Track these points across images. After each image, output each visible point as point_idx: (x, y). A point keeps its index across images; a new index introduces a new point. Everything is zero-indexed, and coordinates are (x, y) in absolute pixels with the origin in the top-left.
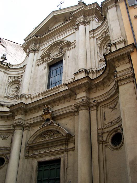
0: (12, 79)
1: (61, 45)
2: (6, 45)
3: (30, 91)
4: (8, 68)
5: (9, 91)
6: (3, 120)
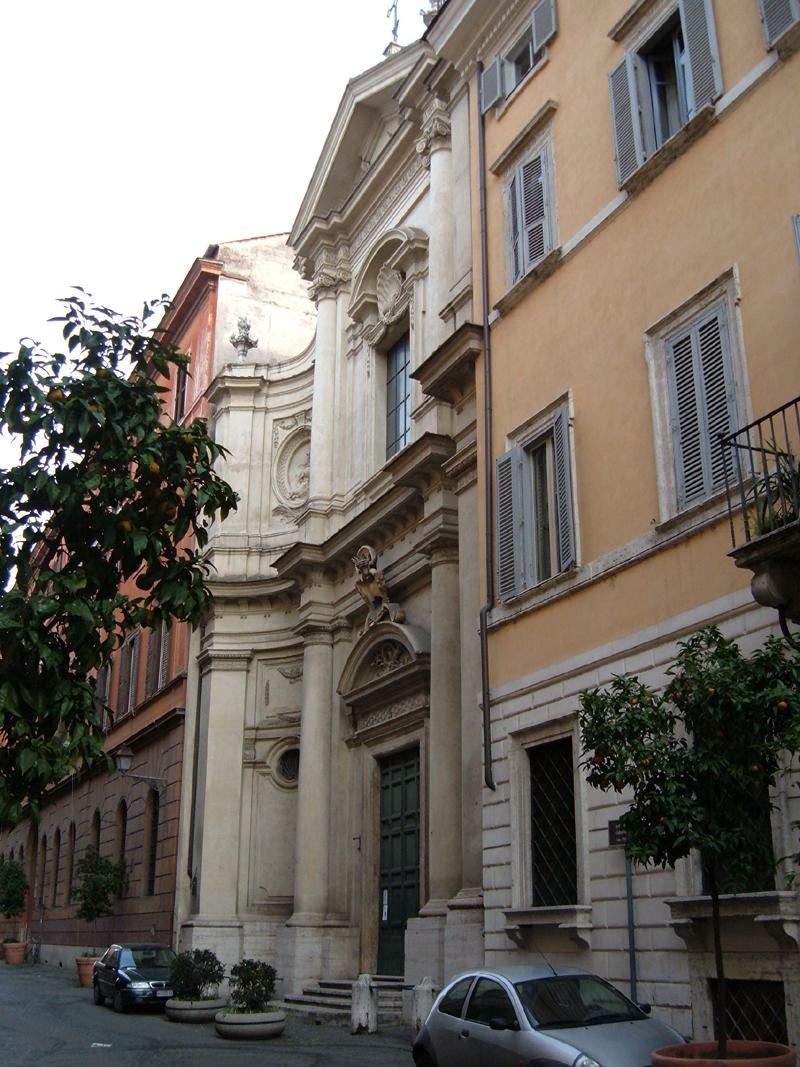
0: (288, 428)
1: (394, 260)
2: (249, 267)
6: (279, 610)
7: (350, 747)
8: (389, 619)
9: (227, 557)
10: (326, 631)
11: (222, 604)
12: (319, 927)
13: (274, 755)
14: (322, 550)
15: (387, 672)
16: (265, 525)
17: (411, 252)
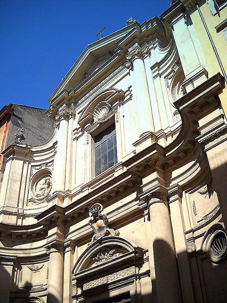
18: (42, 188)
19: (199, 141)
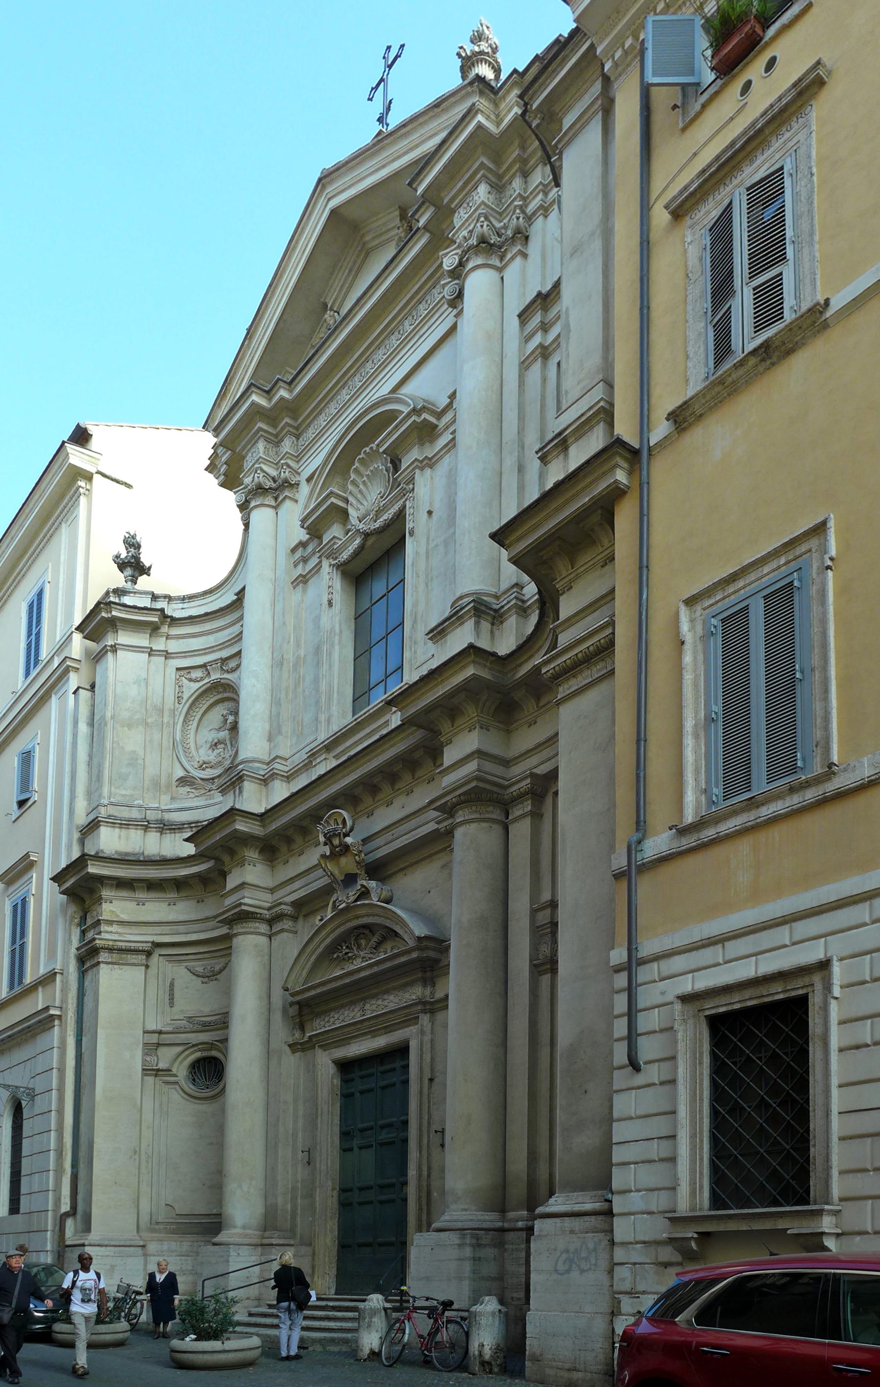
0: (195, 681)
1: (386, 440)
3: (227, 756)
4: (162, 623)
5: (197, 749)
7: (293, 1052)
8: (370, 898)
9: (117, 830)
10: (262, 919)
11: (112, 885)
12: (256, 1245)
13: (181, 1062)
14: (261, 821)
15: (362, 962)
16: (165, 798)
17: (415, 426)
18: (216, 741)
19: (543, 671)
